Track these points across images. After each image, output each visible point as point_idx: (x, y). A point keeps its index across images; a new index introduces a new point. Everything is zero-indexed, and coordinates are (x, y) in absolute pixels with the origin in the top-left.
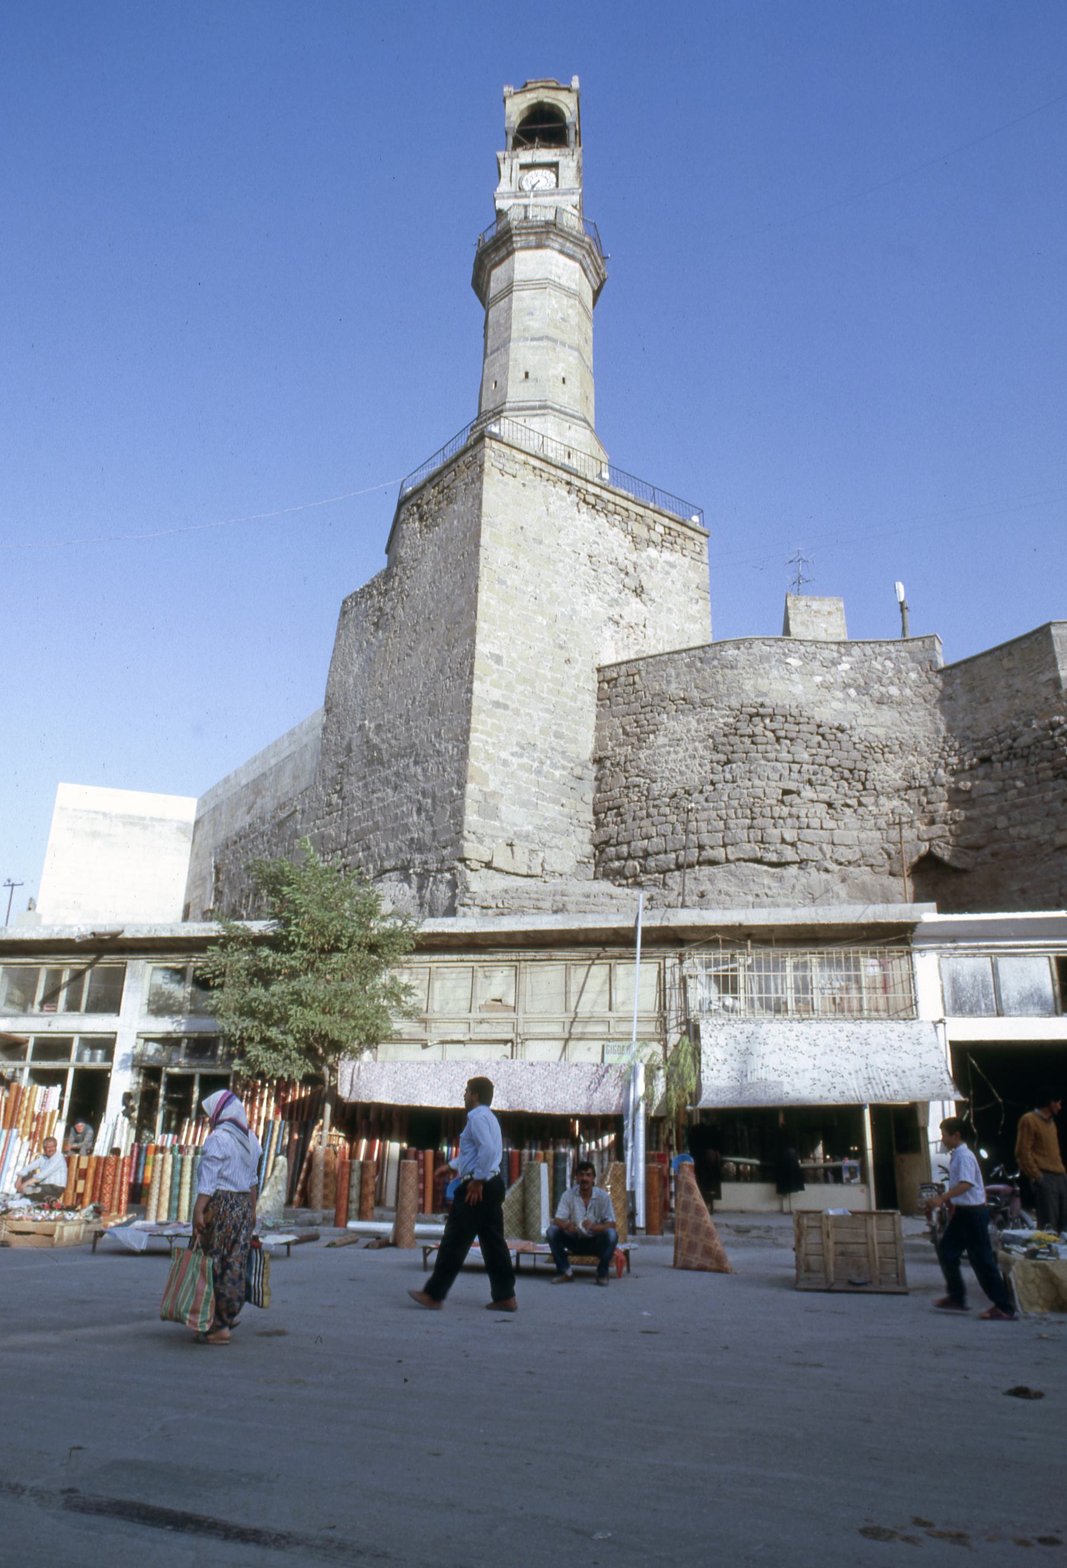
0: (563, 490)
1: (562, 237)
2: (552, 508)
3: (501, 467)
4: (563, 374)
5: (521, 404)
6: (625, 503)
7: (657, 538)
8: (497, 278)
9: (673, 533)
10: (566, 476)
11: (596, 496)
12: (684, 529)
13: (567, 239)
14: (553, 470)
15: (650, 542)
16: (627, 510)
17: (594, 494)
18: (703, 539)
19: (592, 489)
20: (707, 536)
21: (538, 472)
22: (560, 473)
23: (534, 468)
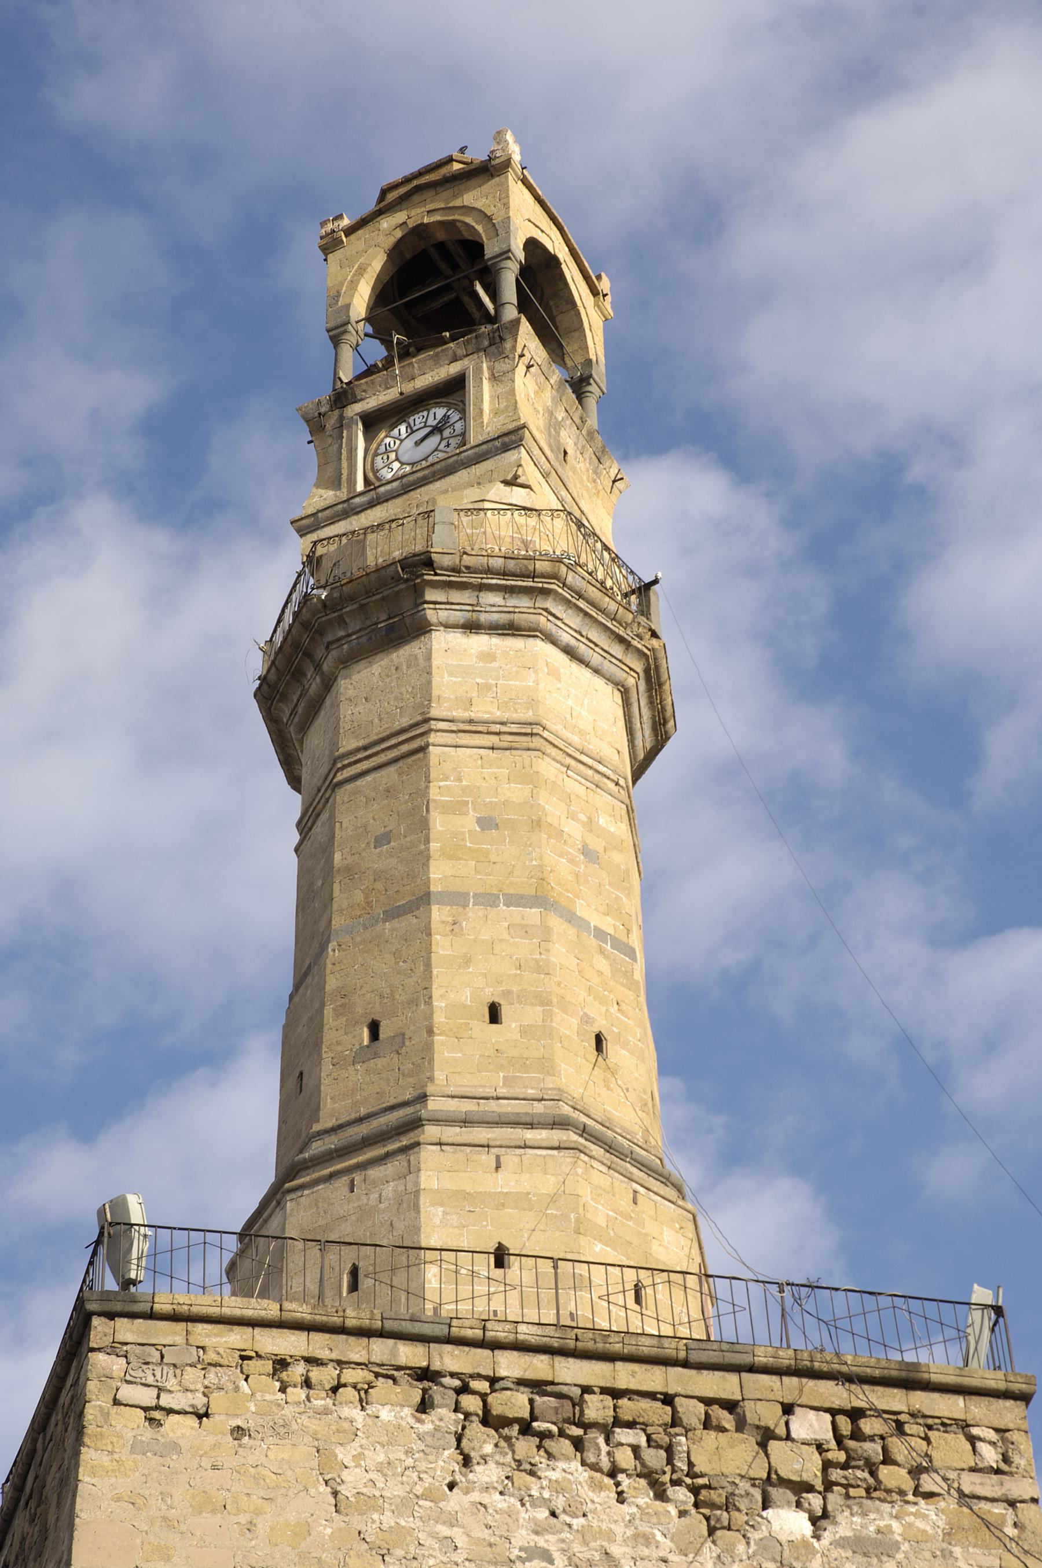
0: (393, 1407)
1: (462, 586)
2: (353, 1481)
3: (147, 1397)
4: (490, 994)
5: (492, 1106)
6: (653, 1378)
7: (798, 1463)
8: (364, 696)
9: (867, 1426)
10: (409, 1354)
11: (537, 1386)
12: (920, 1400)
13: (481, 588)
14: (356, 1350)
15: (771, 1485)
16: (668, 1400)
17: (521, 1382)
18: (1009, 1413)
19: (510, 1365)
20: (1025, 1398)
21: (298, 1370)
22: (380, 1350)
23: (281, 1364)
